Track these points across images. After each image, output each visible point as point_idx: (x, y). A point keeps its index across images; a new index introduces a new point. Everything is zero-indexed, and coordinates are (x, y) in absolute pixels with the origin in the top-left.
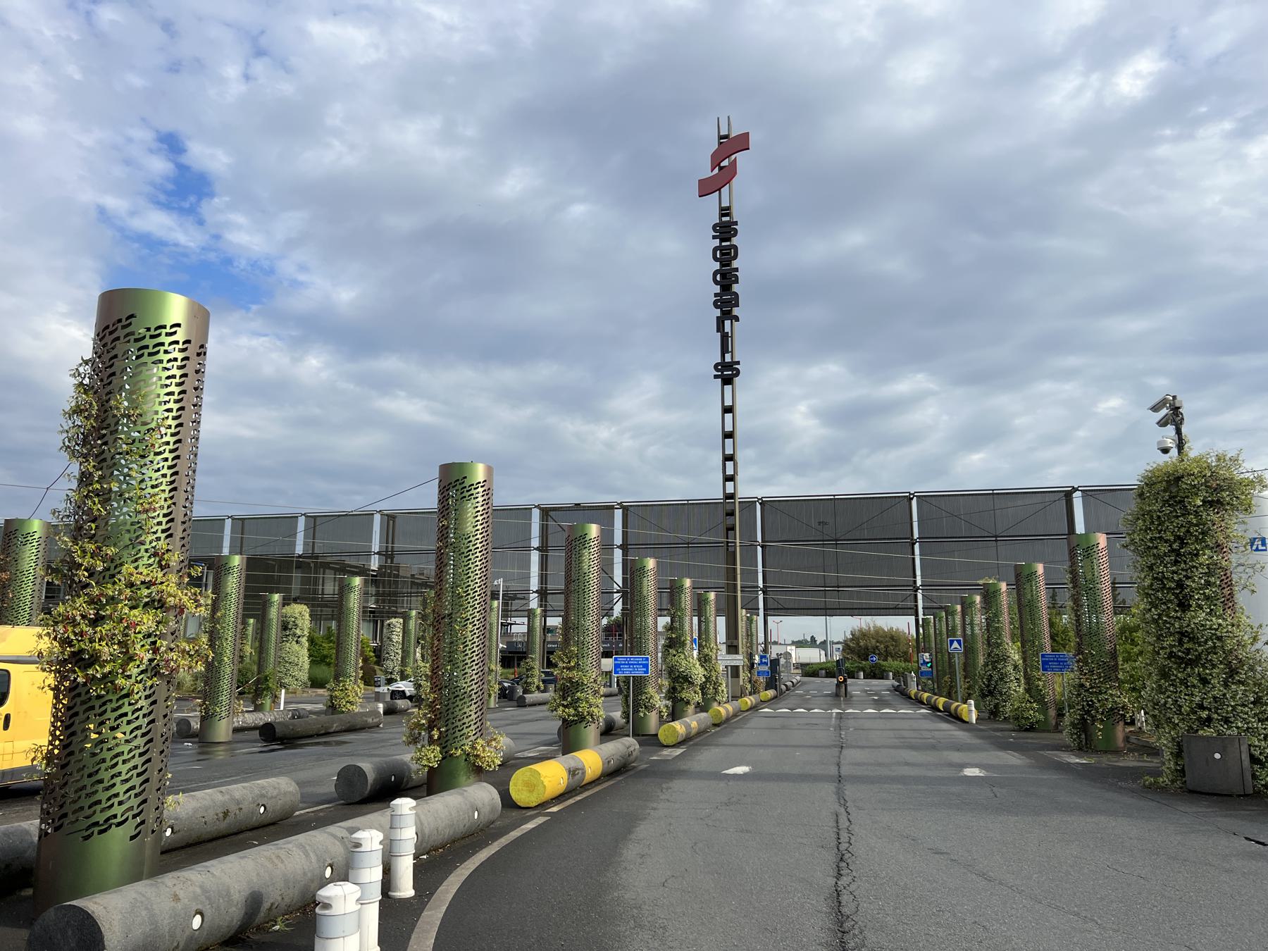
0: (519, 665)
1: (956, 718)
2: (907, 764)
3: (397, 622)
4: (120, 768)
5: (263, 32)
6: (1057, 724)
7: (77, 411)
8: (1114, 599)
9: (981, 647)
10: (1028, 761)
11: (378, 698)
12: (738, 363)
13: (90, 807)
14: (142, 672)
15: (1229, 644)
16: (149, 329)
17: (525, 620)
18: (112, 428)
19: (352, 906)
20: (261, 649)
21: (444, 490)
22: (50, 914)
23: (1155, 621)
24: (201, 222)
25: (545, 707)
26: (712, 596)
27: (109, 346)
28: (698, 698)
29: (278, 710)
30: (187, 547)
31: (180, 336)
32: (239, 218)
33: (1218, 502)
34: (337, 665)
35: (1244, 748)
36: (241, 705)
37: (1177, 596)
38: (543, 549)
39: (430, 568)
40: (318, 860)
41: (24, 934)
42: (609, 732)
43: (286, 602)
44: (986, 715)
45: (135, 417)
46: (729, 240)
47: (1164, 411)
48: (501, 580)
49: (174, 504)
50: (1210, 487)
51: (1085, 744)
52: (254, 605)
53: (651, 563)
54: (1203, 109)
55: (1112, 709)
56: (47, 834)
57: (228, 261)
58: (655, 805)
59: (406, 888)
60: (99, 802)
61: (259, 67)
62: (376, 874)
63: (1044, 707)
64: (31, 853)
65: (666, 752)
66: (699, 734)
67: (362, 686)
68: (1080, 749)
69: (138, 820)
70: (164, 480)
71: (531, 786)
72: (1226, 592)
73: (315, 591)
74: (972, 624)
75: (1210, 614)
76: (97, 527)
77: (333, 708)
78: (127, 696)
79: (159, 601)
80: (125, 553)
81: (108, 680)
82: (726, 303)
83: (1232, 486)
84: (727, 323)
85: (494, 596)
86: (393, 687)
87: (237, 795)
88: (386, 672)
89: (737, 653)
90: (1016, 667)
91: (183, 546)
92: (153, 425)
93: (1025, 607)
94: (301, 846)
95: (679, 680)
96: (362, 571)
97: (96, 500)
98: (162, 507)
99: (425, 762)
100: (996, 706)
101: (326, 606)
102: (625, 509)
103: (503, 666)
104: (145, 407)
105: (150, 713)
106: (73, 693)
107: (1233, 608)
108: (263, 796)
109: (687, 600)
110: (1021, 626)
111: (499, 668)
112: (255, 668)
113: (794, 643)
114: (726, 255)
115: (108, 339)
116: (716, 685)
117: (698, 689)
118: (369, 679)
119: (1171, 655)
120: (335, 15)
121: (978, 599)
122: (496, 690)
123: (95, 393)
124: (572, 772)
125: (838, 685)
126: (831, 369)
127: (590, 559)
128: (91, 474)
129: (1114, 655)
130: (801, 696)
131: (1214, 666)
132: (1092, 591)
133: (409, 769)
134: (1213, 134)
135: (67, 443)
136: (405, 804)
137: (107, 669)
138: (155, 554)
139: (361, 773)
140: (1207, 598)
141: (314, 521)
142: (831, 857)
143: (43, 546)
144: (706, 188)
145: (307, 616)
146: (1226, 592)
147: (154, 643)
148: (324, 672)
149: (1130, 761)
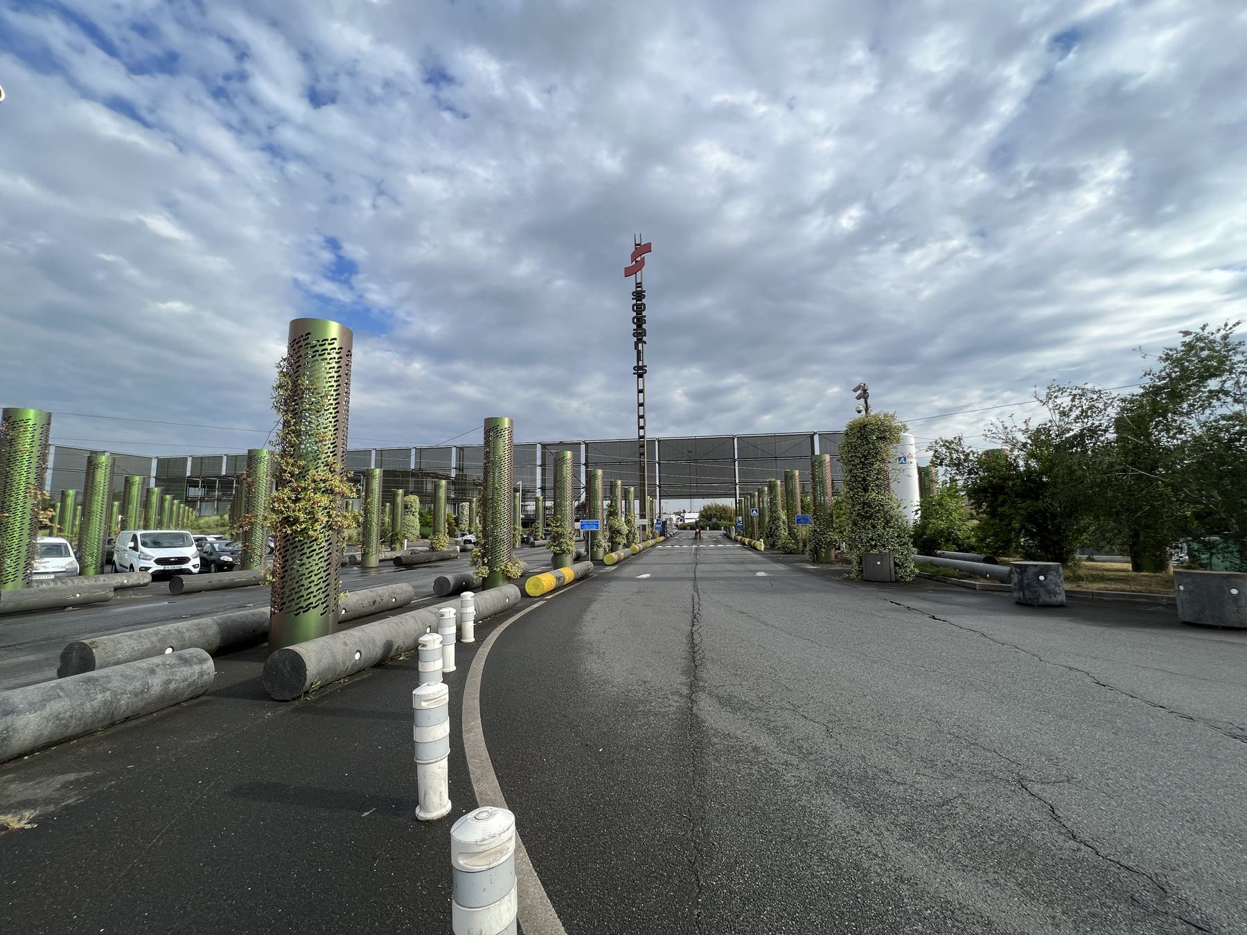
0: (531, 527)
1: (754, 548)
2: (729, 571)
3: (466, 504)
4: (313, 578)
5: (383, 181)
6: (803, 550)
7: (280, 386)
8: (833, 489)
9: (767, 513)
10: (789, 568)
11: (457, 543)
12: (646, 366)
13: (298, 599)
14: (324, 527)
15: (886, 508)
16: (318, 341)
17: (534, 503)
18: (300, 396)
19: (438, 646)
20: (394, 519)
21: (487, 432)
22: (276, 654)
23: (851, 498)
24: (352, 288)
25: (544, 547)
26: (632, 489)
27: (297, 351)
28: (625, 541)
29: (403, 550)
30: (345, 461)
31: (336, 345)
32: (373, 286)
33: (884, 438)
34: (434, 526)
35: (892, 559)
36: (383, 548)
37: (862, 485)
38: (543, 465)
39: (481, 475)
40: (423, 624)
41: (262, 665)
42: (578, 558)
43: (406, 494)
44: (769, 547)
45: (314, 391)
46: (641, 300)
47: (860, 392)
48: (520, 482)
49: (337, 437)
50: (880, 430)
51: (815, 561)
52: (388, 496)
53: (600, 472)
54: (883, 237)
55: (829, 542)
56: (275, 613)
57: (368, 310)
58: (601, 594)
59: (470, 637)
60: (303, 596)
61: (381, 201)
62: (453, 630)
63: (797, 542)
64: (267, 624)
65: (607, 568)
66: (625, 559)
67: (448, 537)
68: (814, 562)
69: (325, 605)
70: (331, 424)
71: (536, 586)
72: (886, 482)
73: (422, 488)
74: (763, 502)
75: (878, 493)
76: (294, 450)
77: (433, 549)
78: (315, 540)
79: (331, 490)
80: (310, 464)
81: (304, 532)
82: (640, 334)
83: (890, 429)
84: (640, 345)
85: (516, 490)
86: (465, 538)
87: (380, 592)
88: (461, 530)
89: (645, 518)
90: (784, 522)
91: (343, 460)
92: (323, 394)
93: (789, 493)
94: (413, 617)
95: (615, 532)
96: (447, 478)
97: (293, 435)
98: (330, 440)
99: (480, 575)
100: (774, 542)
101: (428, 496)
102: (587, 445)
103: (523, 527)
104: (318, 384)
105: (329, 549)
106: (285, 540)
107: (889, 490)
108: (394, 593)
109: (619, 492)
110: (787, 503)
111: (521, 528)
112: (391, 528)
113: (674, 513)
114: (639, 309)
115: (296, 346)
116: (634, 534)
117: (624, 537)
118: (451, 534)
119: (859, 514)
120: (423, 171)
121: (766, 489)
122: (520, 539)
123: (290, 376)
124: (558, 579)
125: (696, 534)
126: (694, 372)
127: (567, 470)
128: (289, 421)
129: (831, 515)
130: (678, 539)
131: (879, 519)
132: (822, 482)
133: (472, 578)
134: (888, 250)
135: (275, 405)
136: (468, 595)
137: (303, 526)
138: (327, 465)
139: (446, 580)
140: (877, 485)
141: (420, 451)
142: (689, 617)
143: (270, 464)
144: (629, 272)
145: (418, 502)
146: (886, 482)
147: (329, 512)
148: (428, 530)
149: (838, 567)
